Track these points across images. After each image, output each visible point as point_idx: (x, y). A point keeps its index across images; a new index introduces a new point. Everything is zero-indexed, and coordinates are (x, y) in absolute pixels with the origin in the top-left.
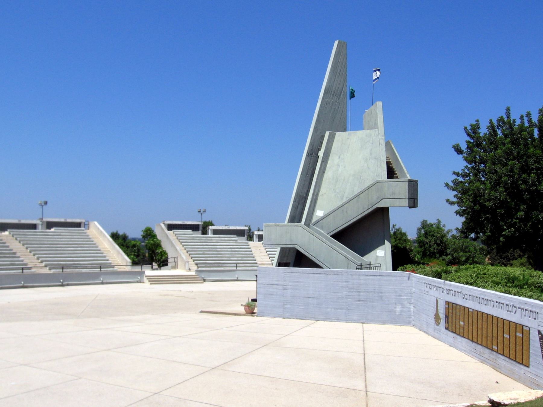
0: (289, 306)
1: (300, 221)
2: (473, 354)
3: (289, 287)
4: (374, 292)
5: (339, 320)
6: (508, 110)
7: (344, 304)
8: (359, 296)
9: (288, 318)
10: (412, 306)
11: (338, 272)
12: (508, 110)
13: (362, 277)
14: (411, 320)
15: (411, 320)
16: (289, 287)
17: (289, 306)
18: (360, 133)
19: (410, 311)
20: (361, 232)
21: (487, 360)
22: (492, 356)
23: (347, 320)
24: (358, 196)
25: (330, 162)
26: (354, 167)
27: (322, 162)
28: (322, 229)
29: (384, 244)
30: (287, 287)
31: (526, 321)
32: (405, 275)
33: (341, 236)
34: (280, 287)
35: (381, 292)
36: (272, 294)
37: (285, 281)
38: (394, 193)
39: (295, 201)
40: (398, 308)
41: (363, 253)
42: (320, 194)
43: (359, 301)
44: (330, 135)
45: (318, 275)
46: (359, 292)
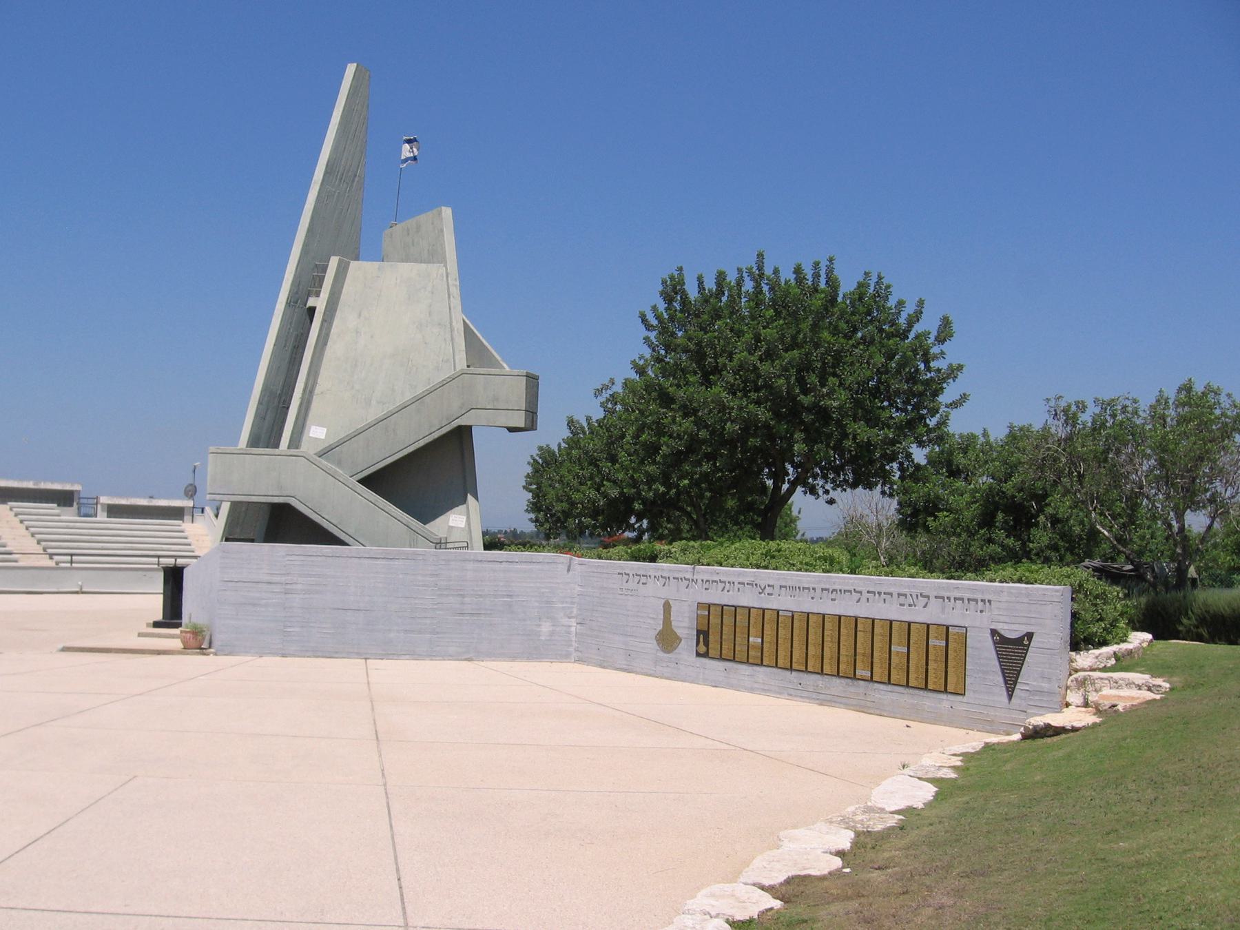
0: (297, 629)
1: (277, 446)
2: (792, 692)
3: (299, 587)
4: (496, 596)
5: (414, 655)
6: (760, 256)
7: (428, 621)
8: (463, 603)
9: (294, 656)
10: (573, 622)
11: (415, 553)
12: (760, 256)
13: (470, 566)
14: (571, 649)
15: (571, 649)
16: (299, 587)
17: (297, 629)
18: (408, 270)
19: (569, 633)
20: (423, 477)
21: (839, 700)
22: (852, 689)
23: (431, 656)
24: (419, 399)
25: (337, 322)
26: (397, 335)
27: (324, 321)
28: (339, 463)
29: (464, 501)
30: (294, 587)
31: (954, 616)
32: (561, 560)
33: (380, 481)
34: (277, 588)
35: (510, 596)
36: (254, 605)
37: (288, 574)
38: (496, 399)
39: (260, 403)
40: (546, 628)
41: (425, 521)
42: (318, 390)
43: (462, 614)
44: (339, 265)
45: (370, 561)
46: (463, 596)
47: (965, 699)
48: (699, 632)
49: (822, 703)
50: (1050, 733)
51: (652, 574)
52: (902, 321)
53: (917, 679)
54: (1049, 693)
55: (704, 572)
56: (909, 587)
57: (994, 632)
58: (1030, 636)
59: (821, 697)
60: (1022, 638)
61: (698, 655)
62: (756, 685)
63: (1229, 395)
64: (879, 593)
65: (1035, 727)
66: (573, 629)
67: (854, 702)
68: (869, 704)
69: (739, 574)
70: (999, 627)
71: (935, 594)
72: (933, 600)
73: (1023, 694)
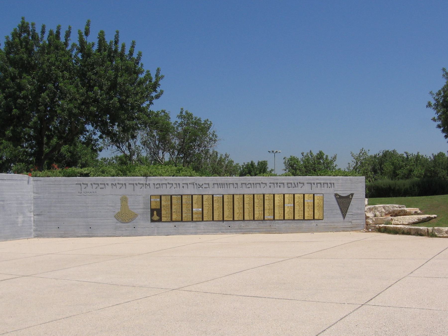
2: (224, 231)
19: (30, 221)
21: (255, 230)
35: (3, 201)
47: (323, 221)
48: (152, 211)
49: (244, 233)
50: (428, 219)
51: (110, 183)
52: (62, 40)
53: (299, 216)
54: (361, 214)
55: (153, 180)
56: (293, 180)
57: (336, 195)
58: (352, 195)
59: (243, 230)
60: (349, 196)
61: (152, 221)
62: (198, 231)
63: (142, 65)
64: (277, 184)
65: (423, 218)
66: (32, 219)
67: (264, 230)
68: (272, 230)
69: (183, 180)
70: (338, 192)
71: (307, 182)
72: (306, 185)
73: (349, 216)
